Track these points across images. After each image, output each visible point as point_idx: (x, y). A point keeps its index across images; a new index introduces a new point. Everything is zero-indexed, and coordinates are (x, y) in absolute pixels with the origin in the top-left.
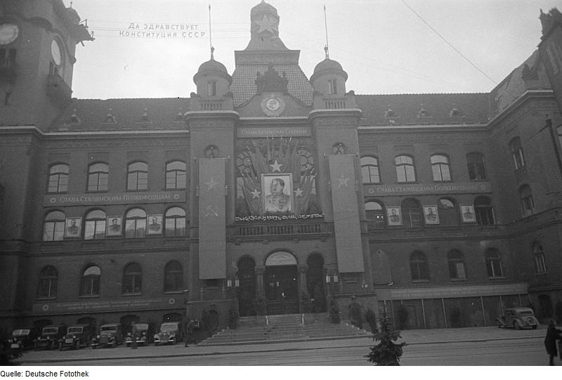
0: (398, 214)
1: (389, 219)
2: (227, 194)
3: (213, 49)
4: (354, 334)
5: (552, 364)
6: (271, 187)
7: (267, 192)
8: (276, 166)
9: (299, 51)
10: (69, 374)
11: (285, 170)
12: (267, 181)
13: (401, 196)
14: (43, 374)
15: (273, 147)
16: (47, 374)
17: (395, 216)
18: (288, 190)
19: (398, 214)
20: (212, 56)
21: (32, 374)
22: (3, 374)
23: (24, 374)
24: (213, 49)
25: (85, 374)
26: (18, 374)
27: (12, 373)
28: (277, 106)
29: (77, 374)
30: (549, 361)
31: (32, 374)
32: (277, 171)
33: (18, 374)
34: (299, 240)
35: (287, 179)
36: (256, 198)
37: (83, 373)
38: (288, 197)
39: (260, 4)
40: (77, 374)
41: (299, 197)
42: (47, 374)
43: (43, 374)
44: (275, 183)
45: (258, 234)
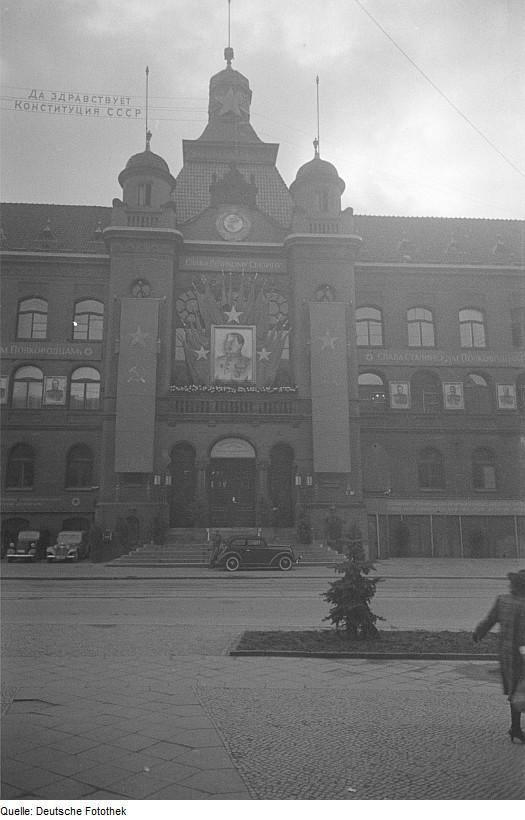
3: (149, 136)
7: (218, 352)
8: (233, 315)
10: (97, 811)
11: (245, 322)
12: (220, 335)
14: (61, 812)
16: (68, 812)
17: (400, 395)
18: (248, 350)
19: (405, 392)
20: (148, 146)
21: (46, 812)
22: (4, 811)
23: (34, 812)
24: (149, 136)
26: (26, 812)
27: (17, 810)
28: (239, 226)
29: (109, 811)
31: (46, 812)
32: (234, 322)
33: (26, 812)
35: (248, 335)
37: (118, 811)
40: (109, 811)
42: (68, 812)
43: (61, 812)
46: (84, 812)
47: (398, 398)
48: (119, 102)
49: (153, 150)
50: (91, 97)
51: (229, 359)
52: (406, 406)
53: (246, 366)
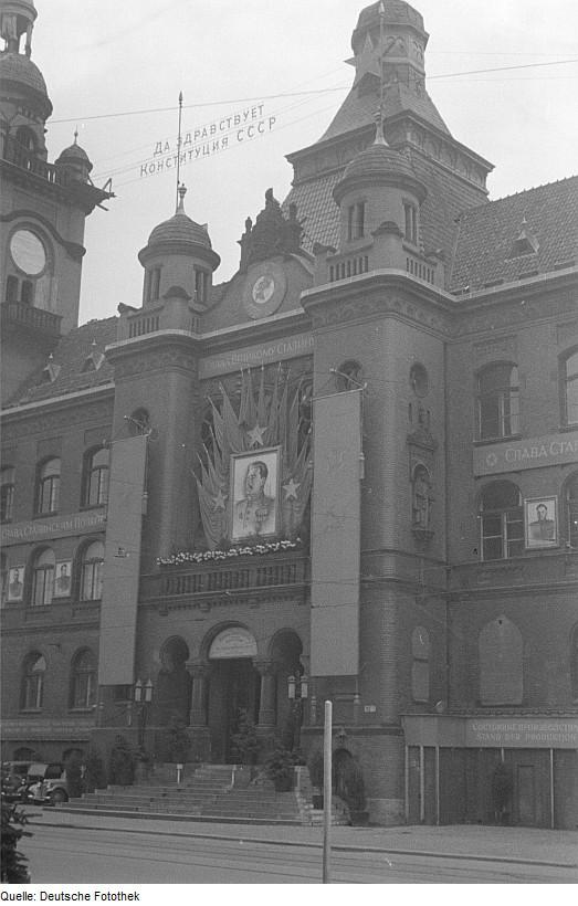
0: (551, 516)
1: (529, 532)
2: (145, 512)
3: (182, 191)
4: (287, 817)
5: (325, 881)
6: (245, 482)
7: (238, 496)
8: (256, 435)
9: (493, 167)
10: (108, 897)
11: (269, 444)
12: (241, 467)
13: (563, 466)
14: (68, 897)
15: (261, 389)
16: (75, 897)
17: (543, 522)
18: (271, 488)
19: (551, 516)
20: (180, 207)
21: (50, 897)
22: (4, 896)
23: (37, 897)
24: (182, 191)
25: (134, 897)
26: (29, 897)
27: (19, 895)
28: (269, 293)
29: (120, 896)
30: (320, 872)
31: (50, 897)
32: (257, 445)
33: (29, 897)
34: (258, 600)
35: (271, 460)
36: (220, 508)
37: (130, 896)
38: (272, 500)
39: (420, 82)
40: (120, 896)
41: (291, 499)
42: (75, 897)
43: (68, 897)
44: (251, 472)
45: (189, 592)
46: (92, 897)
47: (538, 529)
48: (250, 115)
49: (188, 212)
50: (217, 124)
51: (250, 504)
52: (549, 544)
53: (269, 512)
